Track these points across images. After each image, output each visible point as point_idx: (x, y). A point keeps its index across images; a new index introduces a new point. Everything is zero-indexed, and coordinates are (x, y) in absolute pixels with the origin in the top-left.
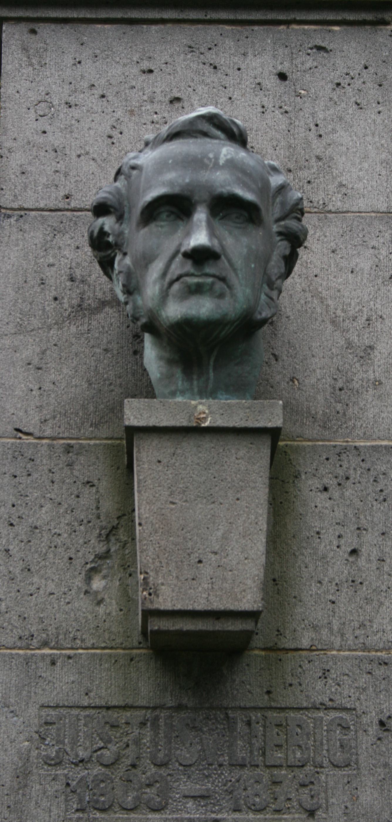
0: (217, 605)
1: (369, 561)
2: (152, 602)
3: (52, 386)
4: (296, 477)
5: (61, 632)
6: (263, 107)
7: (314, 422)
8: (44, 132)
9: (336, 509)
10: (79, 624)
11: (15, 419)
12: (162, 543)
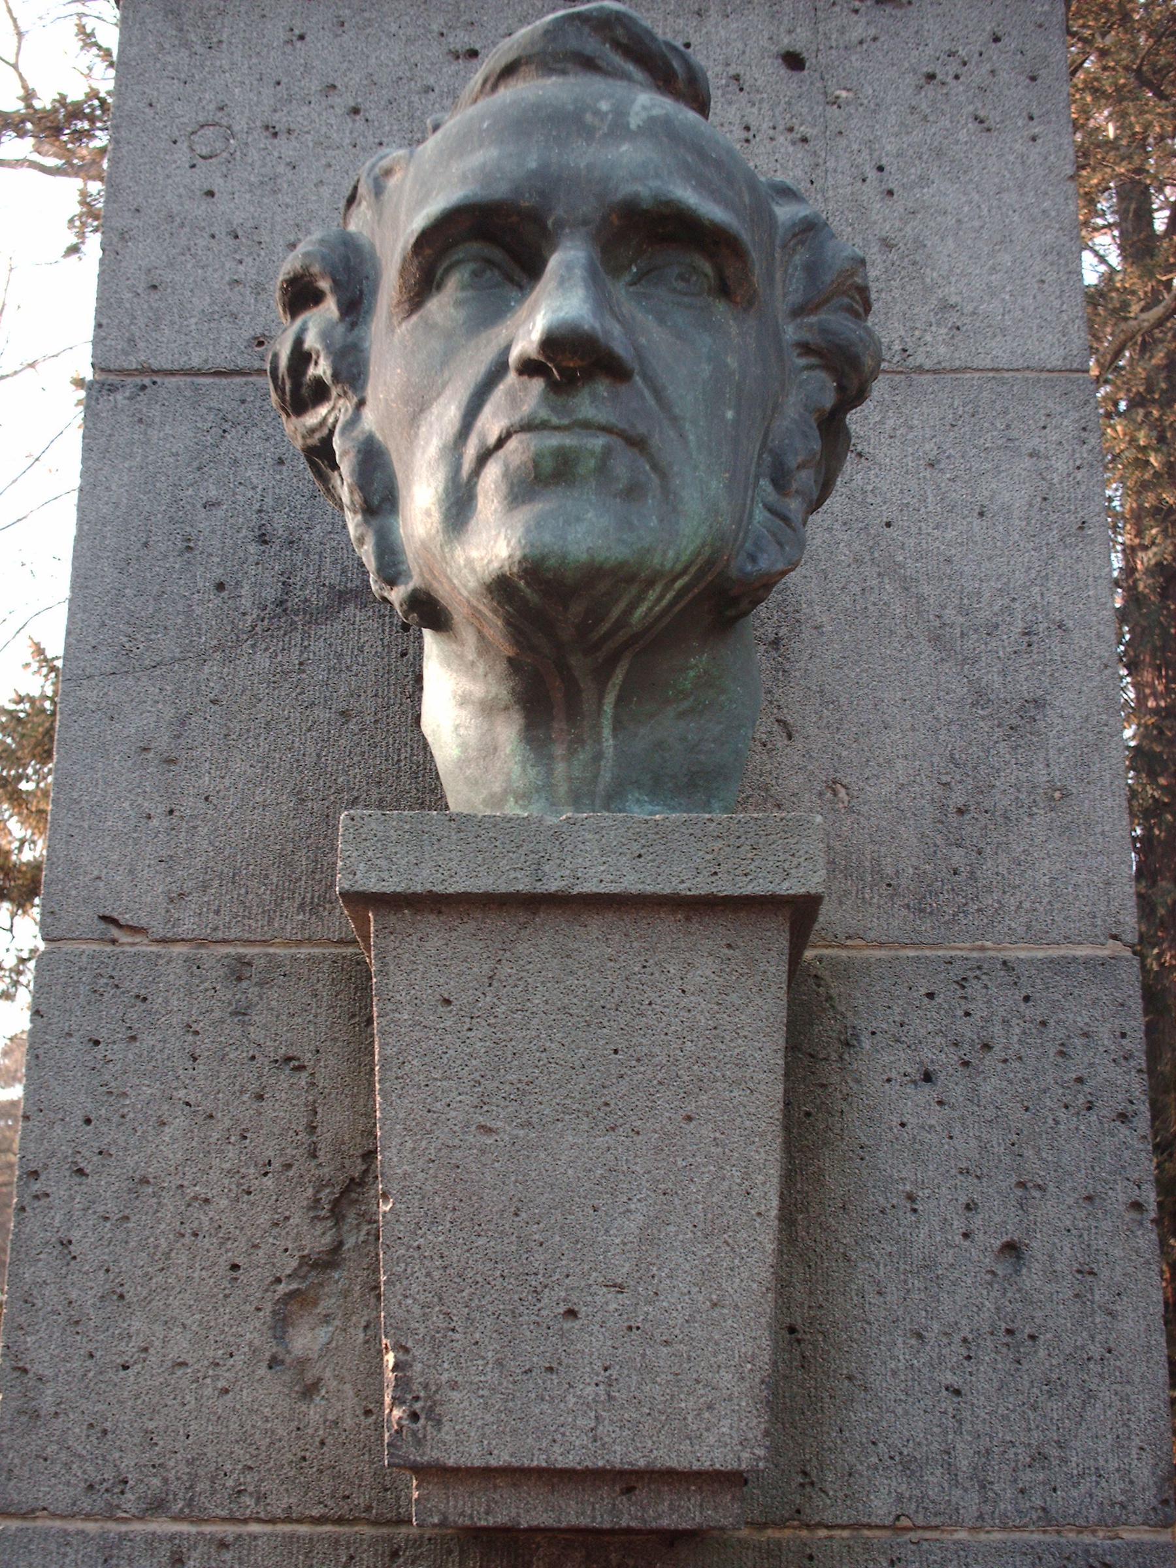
0: (622, 1453)
1: (1053, 1275)
2: (419, 1443)
3: (202, 805)
4: (848, 1044)
5: (201, 1472)
6: (747, 128)
7: (892, 896)
8: (211, 194)
9: (956, 1133)
10: (252, 1450)
11: (102, 891)
12: (454, 1255)
